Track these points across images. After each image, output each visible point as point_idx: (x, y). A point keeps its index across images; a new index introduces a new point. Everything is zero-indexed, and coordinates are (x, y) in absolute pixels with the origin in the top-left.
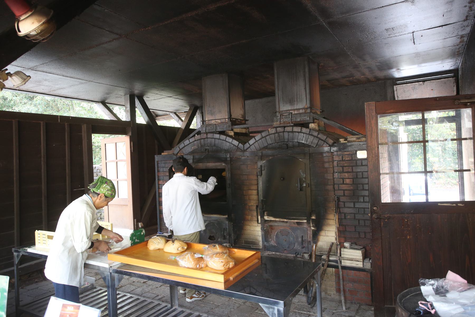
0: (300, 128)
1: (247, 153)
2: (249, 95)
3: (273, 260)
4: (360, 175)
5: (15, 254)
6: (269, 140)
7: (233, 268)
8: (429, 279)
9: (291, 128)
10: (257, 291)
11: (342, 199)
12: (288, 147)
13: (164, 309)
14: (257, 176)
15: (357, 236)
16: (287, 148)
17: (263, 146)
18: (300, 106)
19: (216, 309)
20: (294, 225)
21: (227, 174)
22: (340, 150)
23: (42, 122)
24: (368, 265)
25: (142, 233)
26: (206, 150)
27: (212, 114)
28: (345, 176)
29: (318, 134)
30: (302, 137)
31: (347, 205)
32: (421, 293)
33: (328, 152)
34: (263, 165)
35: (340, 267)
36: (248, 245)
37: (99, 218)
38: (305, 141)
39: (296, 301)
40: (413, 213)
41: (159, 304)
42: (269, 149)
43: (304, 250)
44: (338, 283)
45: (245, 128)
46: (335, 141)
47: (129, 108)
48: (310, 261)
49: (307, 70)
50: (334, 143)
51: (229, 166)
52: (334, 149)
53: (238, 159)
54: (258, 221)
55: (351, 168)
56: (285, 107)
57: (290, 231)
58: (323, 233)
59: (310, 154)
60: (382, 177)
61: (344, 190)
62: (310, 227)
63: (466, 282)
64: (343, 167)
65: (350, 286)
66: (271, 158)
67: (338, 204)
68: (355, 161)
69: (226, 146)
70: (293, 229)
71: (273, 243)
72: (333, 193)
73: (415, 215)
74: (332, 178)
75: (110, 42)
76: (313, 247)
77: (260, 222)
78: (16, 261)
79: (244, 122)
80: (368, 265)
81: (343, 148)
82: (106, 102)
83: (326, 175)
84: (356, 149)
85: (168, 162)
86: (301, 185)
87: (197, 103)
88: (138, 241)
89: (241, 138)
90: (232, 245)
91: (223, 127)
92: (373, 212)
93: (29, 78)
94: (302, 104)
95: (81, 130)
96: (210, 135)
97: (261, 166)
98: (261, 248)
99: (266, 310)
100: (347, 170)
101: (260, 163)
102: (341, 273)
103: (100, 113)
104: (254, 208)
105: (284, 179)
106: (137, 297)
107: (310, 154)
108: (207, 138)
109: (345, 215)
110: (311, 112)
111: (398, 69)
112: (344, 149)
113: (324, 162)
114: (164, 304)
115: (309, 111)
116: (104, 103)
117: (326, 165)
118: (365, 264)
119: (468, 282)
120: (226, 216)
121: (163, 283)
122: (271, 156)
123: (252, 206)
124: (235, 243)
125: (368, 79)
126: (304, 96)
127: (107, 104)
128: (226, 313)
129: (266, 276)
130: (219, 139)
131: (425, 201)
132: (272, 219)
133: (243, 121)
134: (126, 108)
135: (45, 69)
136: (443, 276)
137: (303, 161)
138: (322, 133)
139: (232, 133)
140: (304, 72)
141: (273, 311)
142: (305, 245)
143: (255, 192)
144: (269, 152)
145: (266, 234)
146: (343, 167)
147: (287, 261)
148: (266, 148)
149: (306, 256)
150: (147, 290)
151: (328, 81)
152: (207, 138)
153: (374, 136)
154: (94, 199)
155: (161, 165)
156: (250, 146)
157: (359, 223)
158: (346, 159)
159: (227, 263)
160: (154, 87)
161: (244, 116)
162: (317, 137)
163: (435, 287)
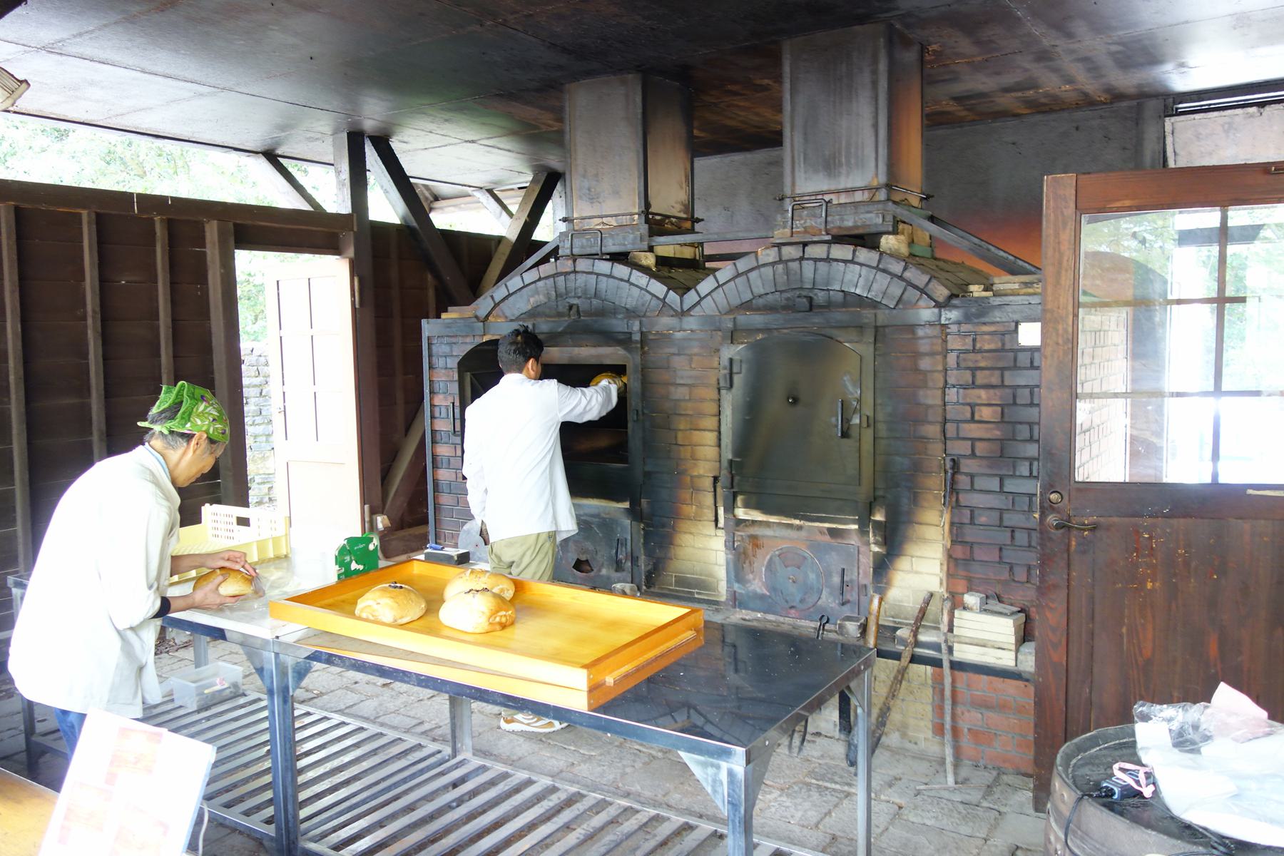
0: (851, 248)
1: (691, 319)
3: (757, 636)
4: (1024, 396)
6: (760, 283)
8: (1161, 703)
9: (825, 247)
10: (708, 721)
11: (968, 466)
12: (811, 306)
14: (719, 390)
15: (1005, 575)
16: (811, 309)
17: (738, 302)
18: (858, 180)
19: (584, 767)
20: (820, 538)
22: (968, 318)
23: (84, 213)
24: (1028, 662)
25: (371, 547)
26: (571, 307)
27: (593, 198)
28: (979, 397)
29: (905, 269)
30: (855, 275)
31: (980, 483)
32: (1135, 742)
33: (931, 324)
34: (737, 358)
35: (946, 664)
36: (685, 590)
37: (266, 499)
38: (863, 289)
39: (816, 754)
41: (419, 746)
42: (758, 309)
44: (939, 710)
45: (692, 245)
46: (955, 292)
47: (346, 175)
48: (861, 643)
49: (883, 66)
51: (638, 359)
52: (951, 315)
53: (664, 338)
54: (716, 520)
55: (998, 373)
56: (808, 183)
57: (808, 553)
58: (903, 564)
59: (876, 327)
61: (973, 440)
62: (868, 544)
63: (1264, 714)
64: (974, 370)
65: (971, 718)
66: (760, 336)
67: (953, 482)
68: (1011, 355)
69: (629, 297)
70: (816, 548)
71: (757, 585)
72: (940, 446)
73: (1174, 521)
74: (939, 402)
76: (871, 601)
77: (721, 523)
79: (688, 225)
80: (1028, 662)
81: (979, 311)
82: (279, 152)
83: (921, 393)
84: (1016, 317)
85: (460, 340)
86: (846, 421)
87: (554, 162)
88: (361, 567)
89: (679, 274)
90: (639, 589)
91: (624, 238)
92: (1047, 507)
93: (24, 85)
94: (866, 173)
95: (203, 238)
96: (583, 265)
97: (731, 360)
98: (723, 599)
99: (695, 768)
100: (985, 381)
101: (731, 351)
103: (261, 188)
104: (708, 483)
105: (796, 401)
107: (876, 327)
108: (575, 272)
109: (972, 512)
110: (888, 199)
111: (1182, 65)
113: (917, 355)
115: (882, 195)
116: (271, 156)
117: (925, 364)
118: (1020, 657)
119: (1271, 717)
120: (626, 505)
121: (434, 689)
122: (759, 330)
123: (699, 477)
124: (650, 581)
125: (1086, 94)
126: (869, 151)
127: (281, 160)
128: (611, 777)
129: (732, 678)
130: (610, 276)
131: (1208, 480)
132: (757, 516)
133: (687, 223)
134: (338, 172)
135: (88, 51)
137: (857, 349)
138: (919, 266)
139: (649, 260)
140: (875, 72)
141: (716, 774)
142: (852, 595)
143: (710, 437)
145: (740, 558)
146: (974, 370)
148: (746, 306)
149: (852, 628)
150: (391, 706)
151: (958, 99)
152: (575, 272)
153: (1066, 280)
154: (174, 455)
156: (702, 299)
157: (1013, 537)
158: (987, 347)
160: (420, 112)
161: (690, 207)
162: (901, 278)
163: (1175, 726)
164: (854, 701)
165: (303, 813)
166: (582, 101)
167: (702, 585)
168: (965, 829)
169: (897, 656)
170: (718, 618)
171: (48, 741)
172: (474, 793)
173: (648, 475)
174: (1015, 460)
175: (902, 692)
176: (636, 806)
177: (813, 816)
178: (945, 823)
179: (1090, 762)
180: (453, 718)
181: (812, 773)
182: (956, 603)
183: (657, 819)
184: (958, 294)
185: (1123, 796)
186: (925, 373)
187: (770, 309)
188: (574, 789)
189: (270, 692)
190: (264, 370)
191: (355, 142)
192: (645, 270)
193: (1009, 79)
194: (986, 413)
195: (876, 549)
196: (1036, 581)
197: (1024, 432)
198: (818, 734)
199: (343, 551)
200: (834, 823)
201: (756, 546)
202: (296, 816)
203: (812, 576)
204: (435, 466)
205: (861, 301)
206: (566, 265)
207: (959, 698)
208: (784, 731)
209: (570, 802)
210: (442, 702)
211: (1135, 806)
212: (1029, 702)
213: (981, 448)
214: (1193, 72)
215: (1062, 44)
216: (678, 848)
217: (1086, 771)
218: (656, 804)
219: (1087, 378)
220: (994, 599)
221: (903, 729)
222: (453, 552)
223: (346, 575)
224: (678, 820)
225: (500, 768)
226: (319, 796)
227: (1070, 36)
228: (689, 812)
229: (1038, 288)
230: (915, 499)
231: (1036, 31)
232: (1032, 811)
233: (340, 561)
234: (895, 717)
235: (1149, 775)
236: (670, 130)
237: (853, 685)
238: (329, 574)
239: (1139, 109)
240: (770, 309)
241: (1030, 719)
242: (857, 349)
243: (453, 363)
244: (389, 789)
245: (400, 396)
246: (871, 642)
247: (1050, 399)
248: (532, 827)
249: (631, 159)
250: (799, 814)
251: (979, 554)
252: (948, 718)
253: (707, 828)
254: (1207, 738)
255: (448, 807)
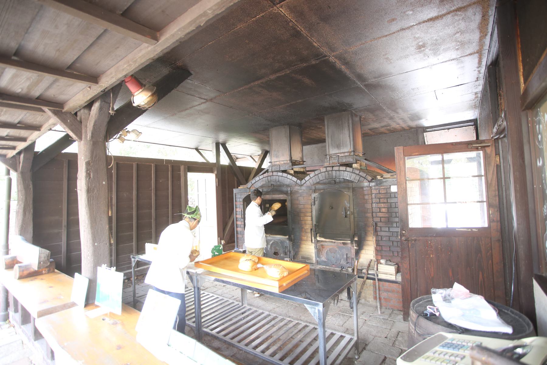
2: (306, 142)
3: (324, 272)
4: (393, 205)
5: (133, 259)
6: (321, 177)
7: (286, 276)
8: (439, 289)
11: (379, 224)
13: (236, 307)
15: (391, 254)
19: (277, 309)
21: (288, 204)
22: (377, 185)
24: (399, 279)
30: (347, 174)
31: (383, 229)
33: (367, 187)
35: (376, 279)
40: (435, 237)
41: (233, 303)
43: (348, 265)
44: (375, 292)
49: (350, 122)
50: (373, 179)
52: (372, 184)
53: (297, 192)
56: (333, 151)
57: (337, 249)
58: (363, 252)
60: (409, 208)
61: (381, 217)
63: (468, 291)
64: (379, 198)
67: (376, 229)
70: (339, 248)
71: (323, 258)
72: (372, 219)
73: (437, 238)
75: (199, 105)
78: (133, 264)
81: (380, 183)
86: (346, 213)
87: (267, 148)
89: (300, 175)
92: (402, 235)
94: (347, 148)
96: (275, 174)
101: (314, 195)
102: (377, 284)
103: (194, 157)
104: (309, 230)
106: (217, 296)
112: (380, 184)
113: (364, 195)
114: (237, 303)
115: (352, 154)
116: (197, 149)
117: (366, 197)
120: (287, 237)
124: (294, 258)
126: (348, 142)
133: (302, 162)
136: (451, 286)
137: (348, 194)
138: (363, 171)
139: (292, 172)
140: (349, 123)
142: (350, 261)
143: (310, 218)
144: (321, 187)
145: (319, 251)
146: (379, 198)
147: (334, 273)
148: (318, 183)
149: (350, 270)
150: (226, 292)
153: (403, 174)
155: (238, 196)
159: (283, 272)
161: (302, 158)
163: (443, 295)
164: (351, 290)
165: (203, 320)
166: (274, 133)
167: (308, 259)
168: (384, 327)
169: (363, 278)
170: (313, 268)
171: (139, 299)
172: (248, 316)
173: (293, 229)
174: (392, 223)
175: (364, 288)
176: (292, 320)
177: (341, 323)
178: (378, 325)
179: (420, 306)
180: (242, 295)
181: (340, 311)
182: (378, 262)
183: (298, 324)
184: (374, 178)
185: (430, 315)
186: (366, 200)
187: (325, 184)
188: (275, 315)
189: (194, 288)
190: (194, 203)
191: (217, 145)
192: (291, 174)
193: (383, 124)
194: (383, 210)
195: (355, 248)
196: (400, 255)
197: (394, 215)
198: (342, 300)
199: (213, 249)
200: (347, 325)
201: (323, 247)
202: (201, 321)
203: (338, 256)
204: (237, 227)
205: (348, 181)
206: (270, 174)
207: (381, 289)
208: (332, 299)
209: (274, 319)
210: (239, 291)
211: (433, 318)
212: (400, 290)
213: (383, 219)
214: (425, 123)
215: (396, 115)
216: (304, 332)
217: (419, 308)
218: (297, 320)
219: (410, 200)
220: (389, 261)
221: (365, 298)
222: (242, 250)
223: (214, 256)
224: (304, 324)
225: (255, 309)
226: (207, 316)
227: (397, 113)
228: (307, 322)
229: (395, 176)
230: (366, 234)
231: (389, 112)
232: (403, 321)
233: (212, 252)
234: (363, 295)
235: (437, 309)
236: (297, 139)
237: (352, 285)
238: (209, 256)
239: (417, 131)
240: (325, 184)
241: (401, 295)
242: (348, 194)
243: (241, 200)
244: (225, 314)
245: (228, 209)
246: (356, 274)
247: (401, 206)
248: (263, 325)
249: (287, 146)
250: (337, 323)
251: (384, 249)
252: (378, 295)
253: (312, 326)
254: (453, 298)
255: (241, 320)
